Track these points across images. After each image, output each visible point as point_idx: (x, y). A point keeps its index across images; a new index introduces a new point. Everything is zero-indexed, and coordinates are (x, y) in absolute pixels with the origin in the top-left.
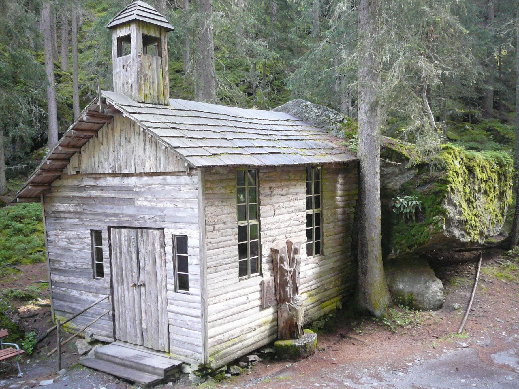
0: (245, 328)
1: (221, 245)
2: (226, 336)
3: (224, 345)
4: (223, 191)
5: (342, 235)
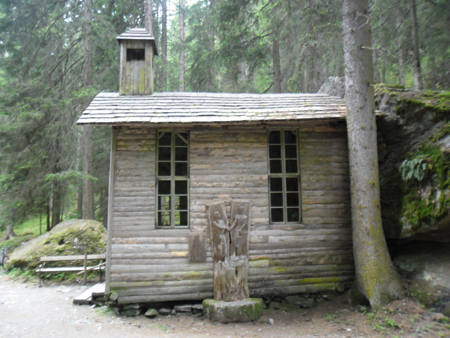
0: (162, 274)
1: (133, 193)
2: (135, 275)
3: (132, 284)
4: (139, 148)
5: (342, 205)
